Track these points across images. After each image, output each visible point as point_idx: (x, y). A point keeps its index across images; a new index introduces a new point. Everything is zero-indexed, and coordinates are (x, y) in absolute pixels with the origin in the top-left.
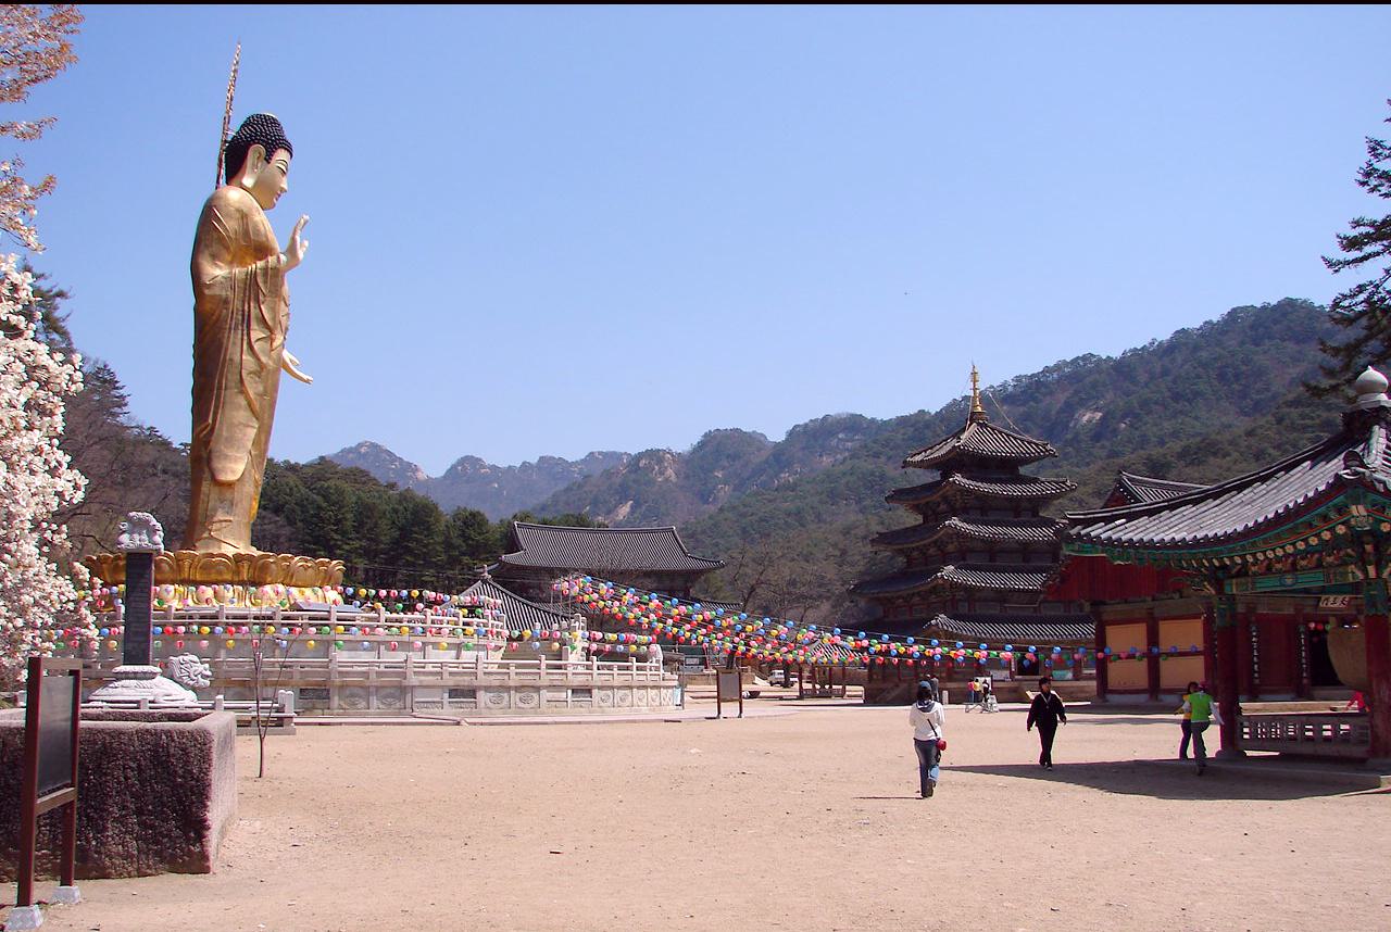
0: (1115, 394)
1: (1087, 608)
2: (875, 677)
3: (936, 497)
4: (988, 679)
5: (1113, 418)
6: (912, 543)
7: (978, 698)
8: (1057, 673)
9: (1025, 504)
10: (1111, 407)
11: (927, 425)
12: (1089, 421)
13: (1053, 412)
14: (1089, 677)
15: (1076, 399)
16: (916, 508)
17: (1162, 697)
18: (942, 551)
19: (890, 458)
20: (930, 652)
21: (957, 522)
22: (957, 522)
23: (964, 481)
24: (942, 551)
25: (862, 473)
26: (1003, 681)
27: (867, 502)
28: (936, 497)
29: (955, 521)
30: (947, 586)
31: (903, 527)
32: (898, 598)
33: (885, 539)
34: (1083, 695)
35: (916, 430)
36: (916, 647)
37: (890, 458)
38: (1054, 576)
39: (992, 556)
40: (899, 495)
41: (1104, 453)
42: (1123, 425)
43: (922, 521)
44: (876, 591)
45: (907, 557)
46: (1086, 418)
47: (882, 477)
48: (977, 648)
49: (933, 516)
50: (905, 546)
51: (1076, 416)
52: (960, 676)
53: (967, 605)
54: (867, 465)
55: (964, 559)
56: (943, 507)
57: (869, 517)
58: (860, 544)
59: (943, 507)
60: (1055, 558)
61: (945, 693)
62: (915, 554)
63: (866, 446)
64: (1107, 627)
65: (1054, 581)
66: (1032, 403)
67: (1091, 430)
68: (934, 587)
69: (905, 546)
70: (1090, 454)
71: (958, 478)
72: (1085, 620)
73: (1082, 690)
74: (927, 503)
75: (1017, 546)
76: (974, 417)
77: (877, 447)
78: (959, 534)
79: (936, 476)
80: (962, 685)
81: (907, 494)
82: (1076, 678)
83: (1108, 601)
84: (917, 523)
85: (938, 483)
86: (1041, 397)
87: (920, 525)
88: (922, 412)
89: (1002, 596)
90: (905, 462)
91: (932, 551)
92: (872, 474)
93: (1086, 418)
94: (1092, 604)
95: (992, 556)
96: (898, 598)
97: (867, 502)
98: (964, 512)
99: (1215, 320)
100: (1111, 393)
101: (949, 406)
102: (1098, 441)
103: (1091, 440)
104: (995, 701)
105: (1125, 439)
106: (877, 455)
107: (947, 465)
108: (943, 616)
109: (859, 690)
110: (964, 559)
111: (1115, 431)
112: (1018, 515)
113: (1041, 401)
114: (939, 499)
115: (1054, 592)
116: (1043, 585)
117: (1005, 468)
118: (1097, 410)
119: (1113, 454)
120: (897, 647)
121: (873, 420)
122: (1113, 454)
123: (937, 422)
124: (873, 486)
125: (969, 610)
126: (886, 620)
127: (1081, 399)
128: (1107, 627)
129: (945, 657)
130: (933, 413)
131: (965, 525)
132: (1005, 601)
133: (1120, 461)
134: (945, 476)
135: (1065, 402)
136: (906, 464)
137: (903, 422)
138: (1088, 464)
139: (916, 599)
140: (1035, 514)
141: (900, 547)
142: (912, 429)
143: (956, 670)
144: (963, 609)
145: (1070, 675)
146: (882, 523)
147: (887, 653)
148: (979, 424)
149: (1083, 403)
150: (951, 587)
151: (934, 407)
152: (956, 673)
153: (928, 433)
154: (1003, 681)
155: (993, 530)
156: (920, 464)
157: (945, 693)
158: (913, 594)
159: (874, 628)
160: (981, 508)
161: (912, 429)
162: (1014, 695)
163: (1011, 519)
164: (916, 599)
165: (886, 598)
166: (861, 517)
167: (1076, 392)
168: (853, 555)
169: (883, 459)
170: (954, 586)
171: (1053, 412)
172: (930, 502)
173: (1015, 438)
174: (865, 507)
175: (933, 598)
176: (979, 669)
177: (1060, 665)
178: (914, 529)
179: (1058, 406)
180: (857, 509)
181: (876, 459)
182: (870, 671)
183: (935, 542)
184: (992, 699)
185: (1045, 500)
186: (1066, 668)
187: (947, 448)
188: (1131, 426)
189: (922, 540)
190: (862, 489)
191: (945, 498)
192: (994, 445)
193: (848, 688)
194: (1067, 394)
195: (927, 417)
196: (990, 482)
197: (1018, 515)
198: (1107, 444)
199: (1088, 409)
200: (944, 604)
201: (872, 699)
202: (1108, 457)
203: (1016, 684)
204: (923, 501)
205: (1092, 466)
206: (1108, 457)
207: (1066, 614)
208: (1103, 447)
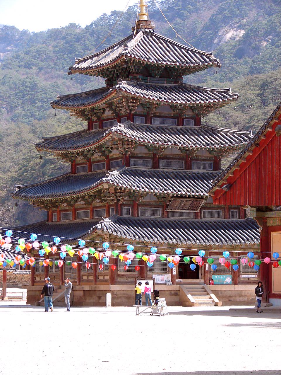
0: (258, 12)
1: (251, 213)
2: (38, 279)
3: (102, 104)
4: (151, 282)
5: (257, 36)
6: (78, 147)
7: (136, 300)
8: (216, 278)
9: (189, 113)
10: (255, 25)
11: (78, 39)
12: (233, 38)
13: (199, 29)
14: (248, 282)
15: (220, 16)
16: (82, 114)
17: (273, 301)
18: (107, 157)
19: (41, 69)
20: (98, 255)
21: (123, 129)
22: (123, 129)
23: (131, 88)
24: (107, 157)
25: (14, 83)
26: (165, 284)
27: (18, 111)
28: (102, 104)
29: (121, 128)
30: (112, 190)
31: (53, 135)
32: (62, 201)
33: (49, 143)
34: (241, 299)
35: (67, 42)
36: (86, 251)
37: (41, 69)
38: (221, 182)
39: (155, 161)
40: (64, 101)
41: (246, 69)
42: (265, 43)
43: (86, 127)
44: (41, 195)
45: (72, 161)
46: (229, 35)
47: (34, 87)
48: (149, 252)
49: (97, 122)
50: (70, 151)
51: (220, 33)
52: (123, 279)
53: (129, 210)
54: (18, 75)
55: (128, 165)
56: (108, 113)
57: (22, 125)
58: (12, 152)
59: (108, 113)
60: (217, 165)
61: (109, 296)
62: (80, 159)
63: (17, 58)
64: (272, 233)
65: (221, 186)
66: (178, 20)
67: (234, 46)
68: (100, 191)
69: (70, 151)
70: (233, 70)
71: (124, 85)
72: (249, 225)
73: (240, 294)
74: (93, 110)
75: (179, 153)
76: (139, 26)
77: (28, 59)
78: (125, 141)
79: (100, 83)
80: (125, 288)
81: (73, 100)
82: (235, 282)
83: (274, 207)
84: (81, 129)
85: (103, 91)
86: (187, 14)
87: (84, 131)
88: (73, 26)
89: (164, 202)
90: (71, 68)
91: (97, 156)
92: (23, 84)
93: (229, 35)
94: (257, 210)
95: (155, 161)
96: (62, 201)
97: (18, 111)
98: (129, 118)
99: (50, 29)
100: (254, 12)
101: (98, 22)
102: (240, 58)
103: (235, 56)
104: (165, 304)
105: (267, 57)
106: (28, 66)
107: (113, 73)
108: (107, 220)
109: (23, 293)
110: (128, 165)
111: (257, 49)
112: (180, 122)
113: (187, 17)
114: (104, 106)
115: (225, 199)
116: (209, 191)
117: (170, 76)
118: (240, 27)
119: (255, 70)
120: (68, 249)
121: (25, 33)
122: (255, 70)
123: (87, 35)
124: (24, 96)
125: (132, 215)
126: (50, 223)
127: (225, 17)
128: (272, 233)
129: (114, 261)
130: (83, 26)
131: (130, 132)
132: (167, 206)
133: (263, 76)
134: (111, 82)
135: (211, 20)
136: (71, 71)
137: (55, 35)
138: (231, 80)
139: (80, 204)
140: (198, 122)
141: (65, 152)
142: (63, 42)
143: (119, 273)
144: (127, 213)
145: (228, 279)
146: (34, 132)
147: (56, 256)
148: (145, 33)
149: (226, 21)
150: (116, 193)
151: (84, 21)
152: (119, 275)
153: (78, 46)
154: (165, 284)
155: (157, 137)
156: (87, 71)
157: (109, 296)
158: (78, 198)
159: (46, 230)
160: (145, 115)
161: (63, 42)
162: (176, 299)
163: (175, 126)
164: (80, 204)
165: (51, 202)
166: (13, 125)
167: (221, 10)
168: (5, 161)
169: (34, 70)
170: (118, 190)
171: (199, 29)
172: (95, 110)
173: (180, 48)
174: (16, 116)
175: (97, 202)
176: (141, 270)
177: (221, 270)
178: (79, 135)
179: (204, 23)
180: (8, 118)
181: (28, 70)
182: (33, 273)
183: (100, 148)
184: (162, 301)
185: (208, 108)
186: (227, 273)
187: (112, 56)
188: (273, 44)
189: (87, 145)
190: (13, 98)
191: (110, 105)
192: (158, 55)
193: (8, 290)
194: (212, 12)
195: (78, 30)
196: (155, 89)
197: (180, 122)
198: (249, 60)
199: (231, 27)
200: (109, 207)
201: (34, 301)
202: (251, 72)
203: (176, 288)
204: (89, 108)
205: (235, 81)
206: (251, 72)
207: (226, 220)
208: (245, 63)
